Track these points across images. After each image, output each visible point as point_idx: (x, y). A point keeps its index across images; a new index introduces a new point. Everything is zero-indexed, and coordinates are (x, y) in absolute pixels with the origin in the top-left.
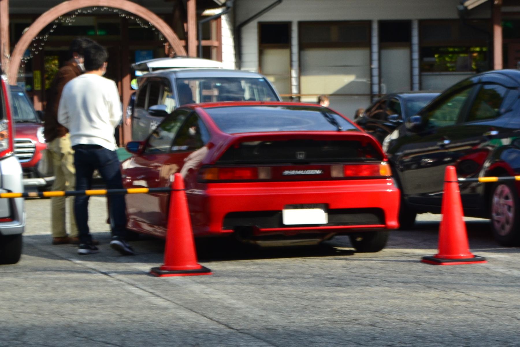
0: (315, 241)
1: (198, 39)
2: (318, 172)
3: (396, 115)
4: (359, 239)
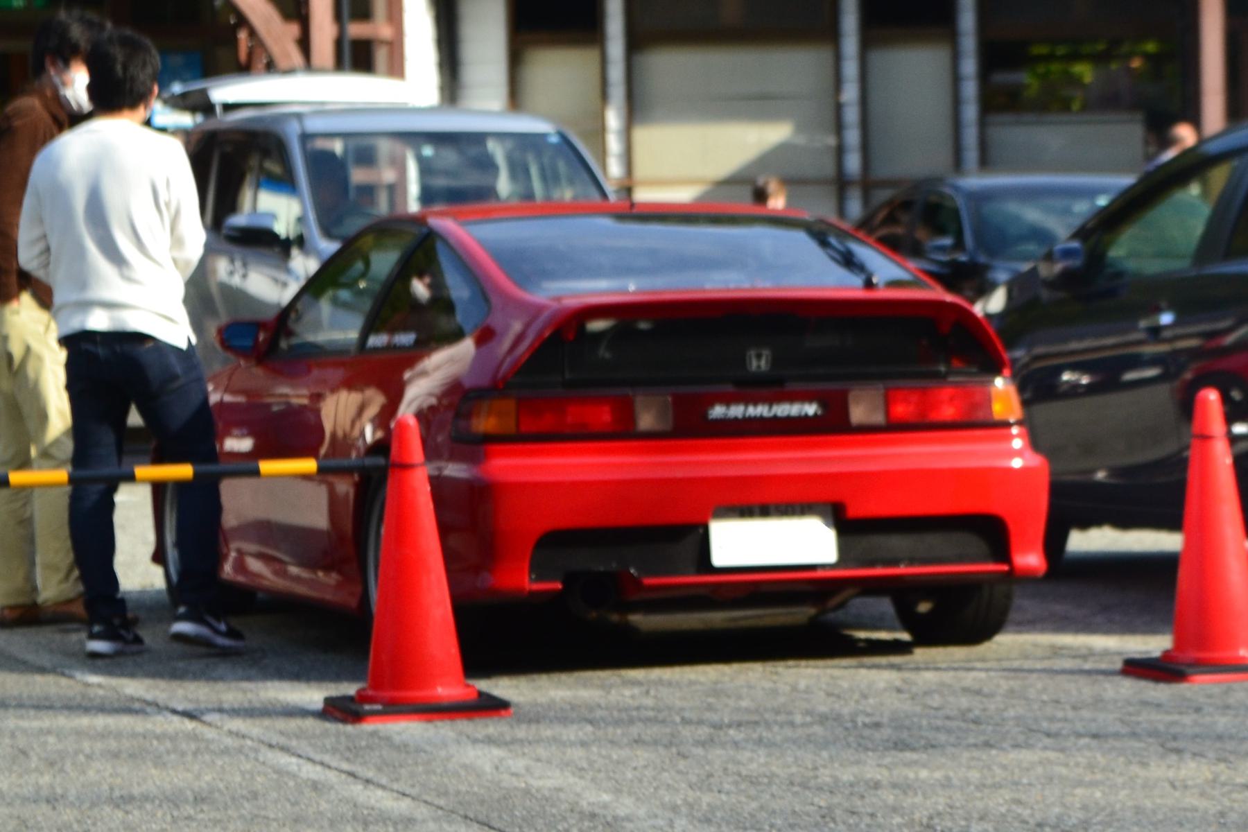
0: (801, 614)
1: (338, 16)
2: (811, 409)
3: (947, 241)
4: (924, 607)
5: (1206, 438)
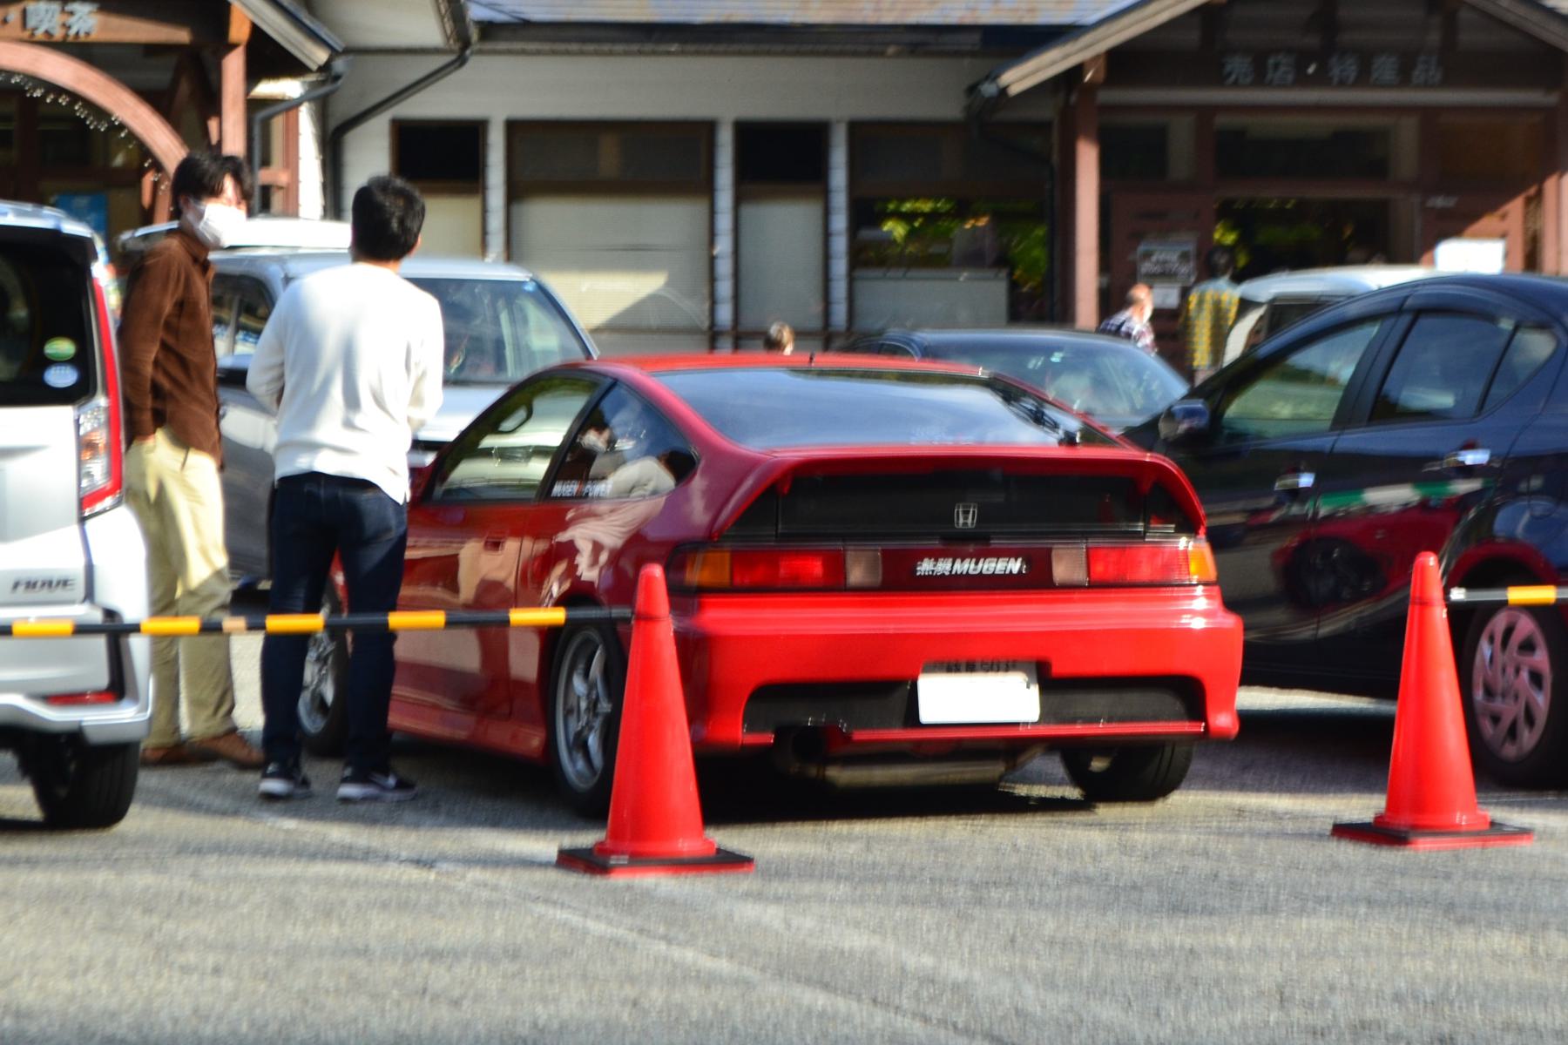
0: (990, 771)
2: (1015, 566)
4: (1098, 765)
5: (1425, 604)
